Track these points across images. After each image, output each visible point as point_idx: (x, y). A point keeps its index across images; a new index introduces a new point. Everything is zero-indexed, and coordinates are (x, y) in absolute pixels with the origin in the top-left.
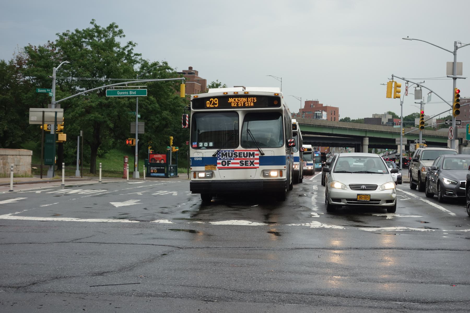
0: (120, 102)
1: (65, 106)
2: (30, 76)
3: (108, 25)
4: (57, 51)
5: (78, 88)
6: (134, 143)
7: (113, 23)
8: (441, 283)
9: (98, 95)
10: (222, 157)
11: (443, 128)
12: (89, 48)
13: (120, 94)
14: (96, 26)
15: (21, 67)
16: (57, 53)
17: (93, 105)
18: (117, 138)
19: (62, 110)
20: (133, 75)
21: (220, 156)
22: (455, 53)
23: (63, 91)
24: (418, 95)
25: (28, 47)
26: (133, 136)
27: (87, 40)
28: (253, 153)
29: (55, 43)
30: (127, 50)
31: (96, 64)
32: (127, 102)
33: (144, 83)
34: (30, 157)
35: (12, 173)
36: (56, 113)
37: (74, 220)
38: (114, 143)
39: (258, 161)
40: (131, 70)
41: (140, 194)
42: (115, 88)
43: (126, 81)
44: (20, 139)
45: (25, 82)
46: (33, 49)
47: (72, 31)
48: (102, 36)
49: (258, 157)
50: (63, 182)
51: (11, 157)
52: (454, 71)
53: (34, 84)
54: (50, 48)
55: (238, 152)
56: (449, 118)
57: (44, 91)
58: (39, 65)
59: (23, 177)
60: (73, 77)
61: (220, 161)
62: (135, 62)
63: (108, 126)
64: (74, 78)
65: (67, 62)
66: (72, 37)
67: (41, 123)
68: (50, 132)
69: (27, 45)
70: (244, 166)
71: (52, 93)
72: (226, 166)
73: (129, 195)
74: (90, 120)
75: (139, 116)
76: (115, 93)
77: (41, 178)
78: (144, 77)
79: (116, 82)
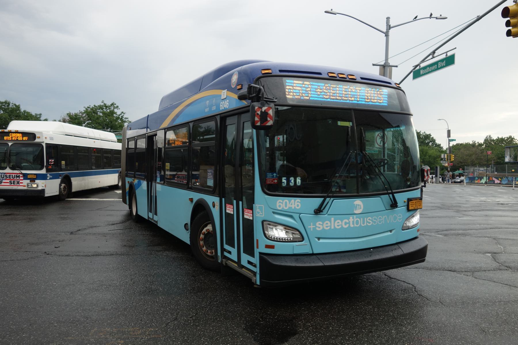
12: (101, 114)
31: (105, 123)
47: (92, 106)
54: (81, 114)
66: (92, 109)
69: (68, 112)
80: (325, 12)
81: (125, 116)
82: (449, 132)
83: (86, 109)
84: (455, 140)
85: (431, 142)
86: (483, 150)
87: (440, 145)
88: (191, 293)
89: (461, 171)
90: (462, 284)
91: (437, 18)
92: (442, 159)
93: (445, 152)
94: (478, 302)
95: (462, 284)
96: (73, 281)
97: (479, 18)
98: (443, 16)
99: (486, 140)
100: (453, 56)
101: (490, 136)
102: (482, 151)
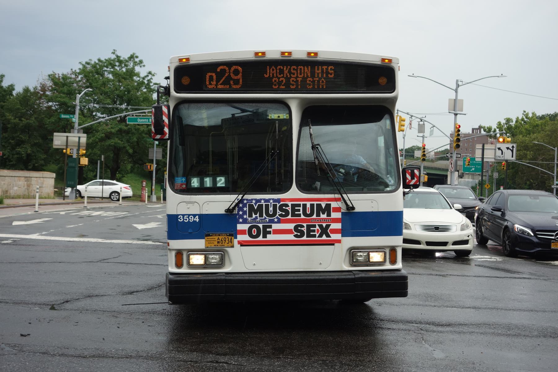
0: (139, 129)
1: (86, 131)
2: (53, 102)
3: (129, 56)
4: (79, 79)
5: (99, 114)
6: (152, 168)
7: (134, 54)
8: (452, 307)
9: (119, 121)
11: (441, 160)
12: (111, 76)
13: (140, 121)
14: (117, 56)
15: (44, 94)
16: (80, 81)
17: (113, 130)
18: (135, 162)
19: (85, 135)
21: (245, 213)
22: (456, 91)
23: (85, 117)
24: (421, 129)
25: (52, 75)
26: (151, 161)
27: (109, 69)
28: (328, 206)
29: (78, 71)
30: (146, 79)
31: (117, 92)
32: (146, 129)
34: (53, 180)
35: (37, 195)
36: (79, 138)
37: (100, 240)
38: (132, 167)
39: (338, 226)
40: (151, 99)
41: (160, 216)
42: (136, 116)
43: (146, 109)
44: (42, 162)
45: (49, 108)
46: (57, 76)
47: (95, 60)
48: (123, 65)
50: (86, 204)
51: (35, 179)
52: (455, 108)
53: (56, 110)
54: (73, 76)
55: (290, 204)
56: (446, 151)
57: (67, 116)
58: (62, 92)
59: (45, 198)
60: (94, 103)
61: (246, 227)
63: (127, 152)
64: (95, 105)
65: (90, 90)
66: (94, 66)
67: (65, 147)
68: (72, 156)
70: (305, 238)
71: (76, 119)
72: (261, 238)
73: (150, 218)
74: (110, 145)
76: (136, 120)
77: (64, 200)
79: (136, 110)
83: (84, 66)
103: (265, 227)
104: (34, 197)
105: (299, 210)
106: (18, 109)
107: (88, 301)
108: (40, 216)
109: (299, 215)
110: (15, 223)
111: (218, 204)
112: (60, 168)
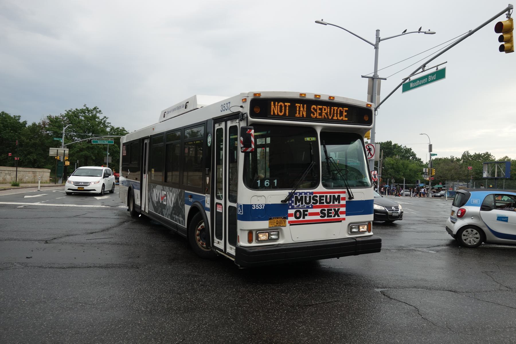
1: (69, 147)
5: (76, 138)
10: (296, 204)
12: (83, 118)
13: (99, 142)
17: (84, 147)
20: (106, 133)
28: (339, 196)
31: (86, 127)
32: (102, 147)
33: (112, 138)
35: (39, 181)
37: (75, 206)
39: (343, 209)
44: (43, 164)
47: (74, 109)
49: (343, 202)
53: (51, 136)
54: (62, 118)
55: (318, 195)
57: (58, 139)
58: (55, 126)
62: (107, 127)
66: (74, 113)
69: (48, 115)
70: (326, 218)
71: (62, 141)
72: (301, 219)
75: (109, 154)
78: (112, 134)
80: (316, 22)
81: (107, 121)
82: (430, 146)
83: (68, 112)
84: (436, 155)
85: (411, 156)
86: (462, 165)
87: (420, 159)
88: (177, 313)
89: (440, 186)
90: (466, 307)
91: (425, 33)
92: (423, 173)
93: (426, 166)
94: (488, 328)
95: (466, 307)
96: (44, 298)
97: (471, 33)
98: (432, 31)
99: (464, 156)
100: (444, 70)
101: (467, 152)
102: (461, 166)
103: (304, 211)
104: (38, 183)
105: (323, 200)
106: (29, 134)
107: (67, 238)
108: (41, 193)
109: (323, 203)
110: (25, 197)
111: (276, 196)
112: (54, 167)
